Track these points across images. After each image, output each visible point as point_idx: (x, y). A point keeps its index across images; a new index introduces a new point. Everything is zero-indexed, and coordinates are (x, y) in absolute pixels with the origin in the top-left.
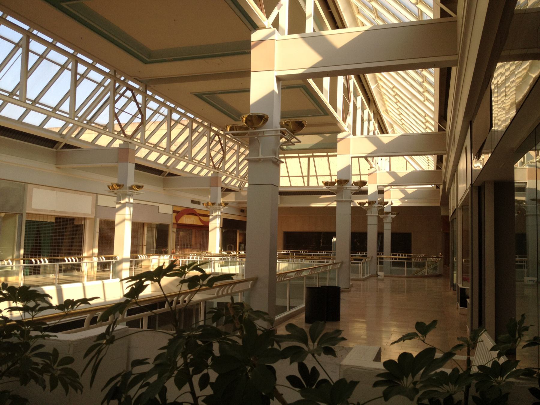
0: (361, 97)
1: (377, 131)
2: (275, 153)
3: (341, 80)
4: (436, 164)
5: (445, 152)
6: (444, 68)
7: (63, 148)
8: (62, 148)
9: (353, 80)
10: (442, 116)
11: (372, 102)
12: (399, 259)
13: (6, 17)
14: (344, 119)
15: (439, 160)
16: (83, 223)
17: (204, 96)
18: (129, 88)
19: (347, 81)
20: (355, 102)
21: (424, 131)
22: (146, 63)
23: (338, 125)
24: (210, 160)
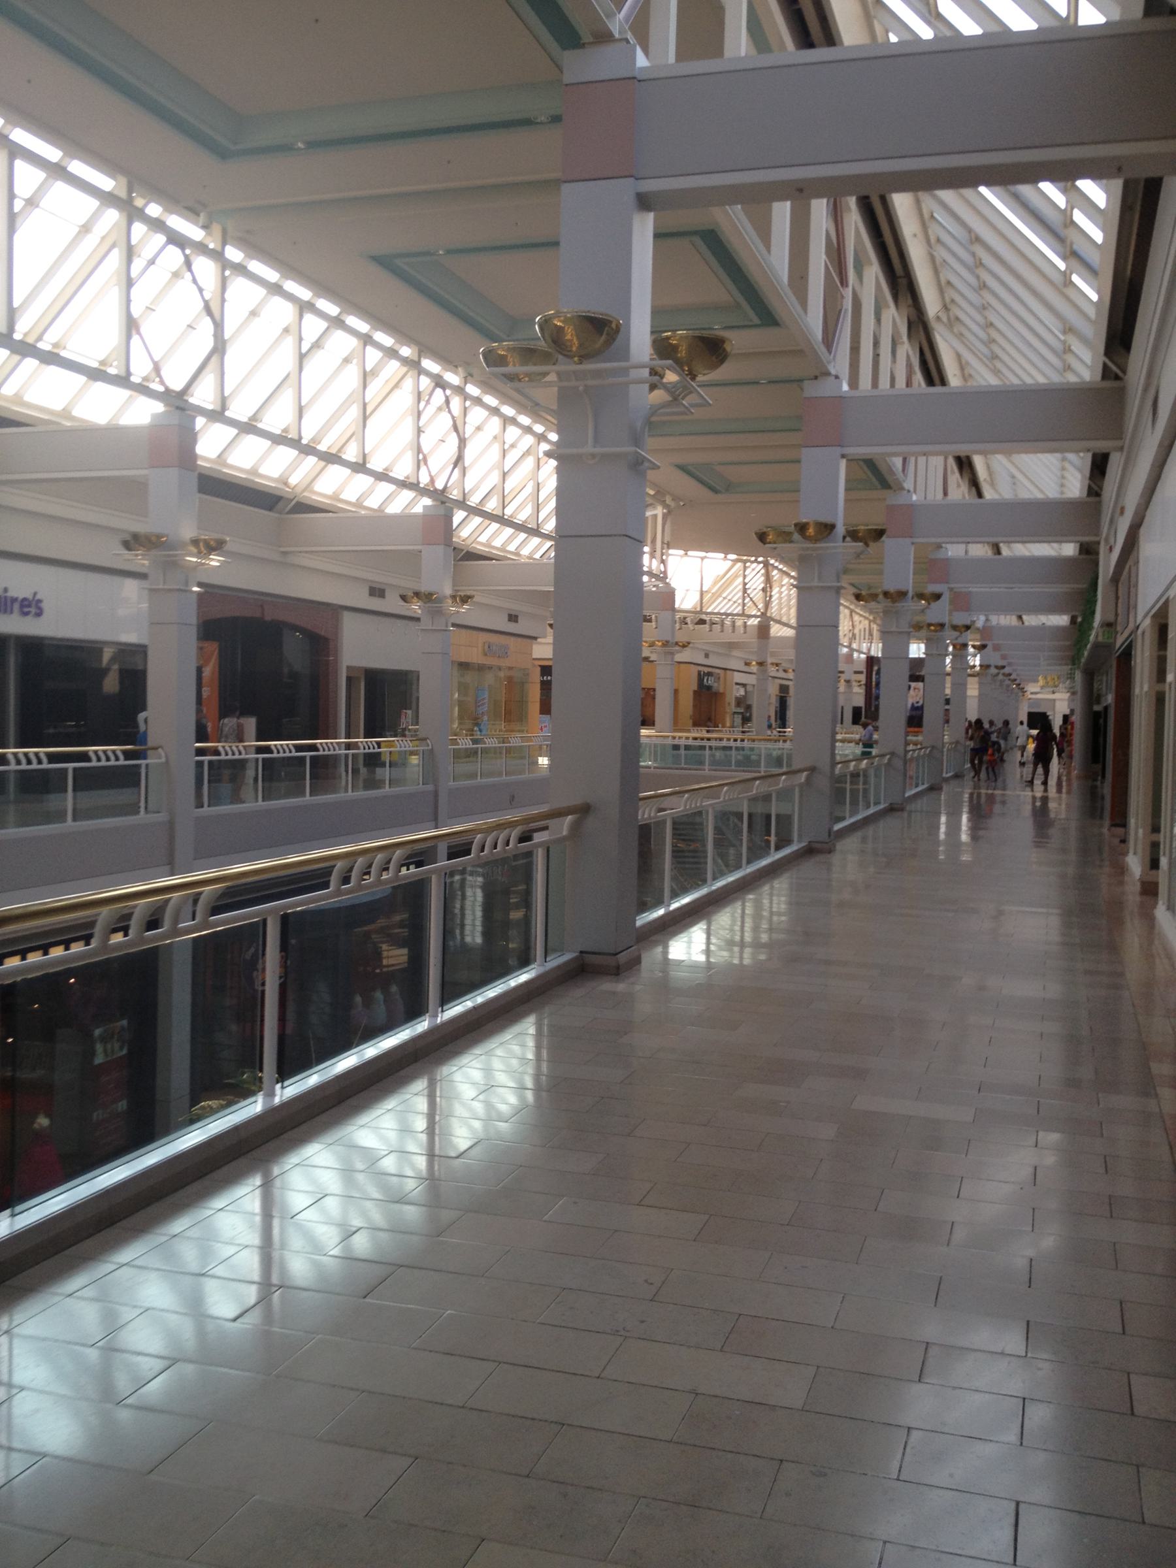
0: (874, 271)
1: (919, 377)
2: (637, 441)
3: (820, 208)
4: (1087, 482)
5: (1118, 443)
7: (290, 512)
13: (146, 205)
14: (829, 340)
15: (1099, 466)
17: (399, 262)
18: (176, 240)
19: (836, 214)
20: (857, 288)
21: (1056, 378)
22: (223, 154)
23: (47, 642)
24: (419, 461)
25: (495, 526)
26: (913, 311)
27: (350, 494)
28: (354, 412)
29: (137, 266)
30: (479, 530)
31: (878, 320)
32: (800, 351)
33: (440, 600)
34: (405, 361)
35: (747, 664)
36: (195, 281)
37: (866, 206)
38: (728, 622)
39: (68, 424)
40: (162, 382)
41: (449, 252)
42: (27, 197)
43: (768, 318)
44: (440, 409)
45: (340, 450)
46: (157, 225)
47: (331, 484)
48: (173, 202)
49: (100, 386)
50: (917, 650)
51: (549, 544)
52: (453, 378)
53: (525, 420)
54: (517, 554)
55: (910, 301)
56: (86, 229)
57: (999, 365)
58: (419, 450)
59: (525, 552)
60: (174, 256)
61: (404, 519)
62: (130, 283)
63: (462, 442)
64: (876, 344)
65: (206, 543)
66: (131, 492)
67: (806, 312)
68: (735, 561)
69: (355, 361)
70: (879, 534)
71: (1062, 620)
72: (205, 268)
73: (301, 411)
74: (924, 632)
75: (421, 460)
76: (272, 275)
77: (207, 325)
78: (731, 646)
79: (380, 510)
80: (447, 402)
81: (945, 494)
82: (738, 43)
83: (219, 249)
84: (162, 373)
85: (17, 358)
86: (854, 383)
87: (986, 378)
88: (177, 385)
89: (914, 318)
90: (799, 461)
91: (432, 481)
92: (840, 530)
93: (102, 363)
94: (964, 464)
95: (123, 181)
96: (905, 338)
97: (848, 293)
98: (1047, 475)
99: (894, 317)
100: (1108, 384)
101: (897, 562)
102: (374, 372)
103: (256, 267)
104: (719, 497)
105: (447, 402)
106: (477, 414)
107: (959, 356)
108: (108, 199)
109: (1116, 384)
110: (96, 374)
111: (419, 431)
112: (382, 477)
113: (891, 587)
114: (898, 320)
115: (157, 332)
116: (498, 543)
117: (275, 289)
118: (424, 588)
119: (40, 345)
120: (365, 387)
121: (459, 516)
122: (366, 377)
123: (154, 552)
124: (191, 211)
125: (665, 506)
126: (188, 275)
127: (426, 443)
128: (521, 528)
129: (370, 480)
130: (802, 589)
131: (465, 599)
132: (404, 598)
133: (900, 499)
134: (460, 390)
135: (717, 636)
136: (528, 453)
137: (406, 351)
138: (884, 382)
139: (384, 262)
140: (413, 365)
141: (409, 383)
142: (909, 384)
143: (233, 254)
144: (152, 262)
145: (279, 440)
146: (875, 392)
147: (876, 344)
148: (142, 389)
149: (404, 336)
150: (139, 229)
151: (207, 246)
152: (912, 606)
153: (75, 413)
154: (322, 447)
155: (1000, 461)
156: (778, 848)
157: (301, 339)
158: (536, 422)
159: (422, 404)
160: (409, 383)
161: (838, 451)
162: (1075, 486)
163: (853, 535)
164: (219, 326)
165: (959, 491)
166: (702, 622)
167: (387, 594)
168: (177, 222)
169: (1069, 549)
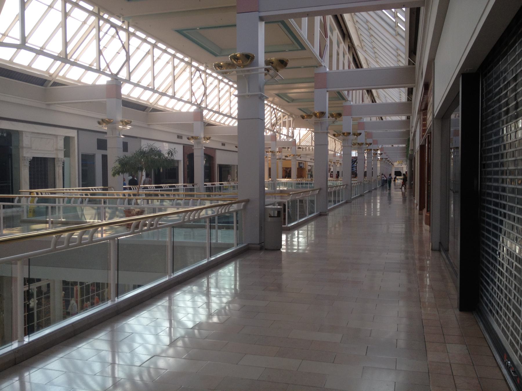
0: (337, 32)
1: (352, 65)
5: (414, 85)
6: (414, 8)
7: (151, 112)
8: (51, 86)
9: (330, 19)
10: (412, 51)
11: (346, 36)
12: (89, 190)
13: (104, 15)
14: (321, 55)
15: (410, 92)
16: (176, 165)
17: (185, 32)
18: (113, 25)
21: (396, 65)
25: (217, 115)
26: (350, 44)
27: (177, 108)
28: (171, 78)
29: (102, 34)
30: (212, 116)
31: (344, 57)
32: (312, 57)
33: (200, 139)
34: (187, 63)
35: (223, 144)
36: (120, 39)
37: (336, 18)
38: (307, 148)
39: (80, 84)
40: (110, 71)
41: (200, 29)
42: (49, 4)
43: (303, 47)
44: (198, 78)
45: (166, 91)
46: (107, 21)
47: (164, 102)
48: (112, 14)
49: (147, 91)
50: (354, 154)
51: (234, 120)
52: (202, 68)
53: (215, 75)
54: (224, 124)
55: (349, 41)
56: (84, 23)
57: (378, 60)
58: (192, 91)
59: (227, 123)
60: (113, 31)
61: (188, 113)
62: (99, 40)
63: (206, 88)
64: (338, 54)
65: (125, 122)
66: (101, 106)
67: (301, 28)
68: (309, 131)
69: (171, 63)
70: (340, 115)
71: (404, 145)
72: (123, 35)
73: (154, 78)
74: (356, 146)
75: (192, 94)
76: (143, 36)
77: (123, 52)
78: (307, 155)
79: (180, 110)
80: (200, 75)
81: (363, 101)
82: (351, 68)
83: (127, 28)
84: (110, 67)
85: (63, 64)
86: (331, 68)
87: (374, 65)
88: (115, 72)
89: (350, 46)
90: (235, 25)
91: (196, 101)
92: (327, 114)
93: (90, 65)
94: (369, 92)
95: (97, 8)
96: (347, 53)
97: (328, 40)
98: (396, 95)
99: (344, 46)
100: (411, 66)
101: (347, 123)
102: (177, 66)
103: (138, 33)
104: (290, 104)
105: (200, 75)
106: (210, 79)
107: (366, 59)
108: (91, 13)
109: (413, 66)
110: (88, 68)
111: (192, 85)
112: (180, 100)
113: (360, 142)
114: (345, 47)
115: (108, 54)
116: (218, 120)
117: (145, 40)
118: (194, 135)
119: (71, 60)
120: (174, 70)
121: (205, 112)
122: (174, 68)
123: (109, 125)
124: (118, 17)
125: (293, 118)
126: (117, 36)
127: (194, 89)
128: (225, 115)
129: (132, 86)
130: (343, 146)
131: (209, 139)
132: (188, 139)
133: (347, 104)
134: (204, 72)
135: (304, 152)
136: (227, 91)
137: (187, 59)
138: (341, 68)
139: (179, 32)
140: (189, 64)
141: (188, 70)
142: (349, 67)
143: (131, 30)
144: (106, 33)
145: (146, 88)
146: (338, 71)
147: (338, 54)
148: (103, 73)
149: (186, 55)
150: (101, 22)
151: (123, 27)
152: (352, 137)
153: (82, 81)
154: (160, 90)
155: (381, 91)
156: (310, 214)
157: (153, 56)
158: (185, 57)
159: (193, 76)
160: (188, 70)
161: (326, 90)
162: (404, 98)
163: (332, 115)
164: (127, 53)
165: (367, 100)
166: (299, 148)
167: (183, 137)
168: (113, 20)
169: (404, 118)
